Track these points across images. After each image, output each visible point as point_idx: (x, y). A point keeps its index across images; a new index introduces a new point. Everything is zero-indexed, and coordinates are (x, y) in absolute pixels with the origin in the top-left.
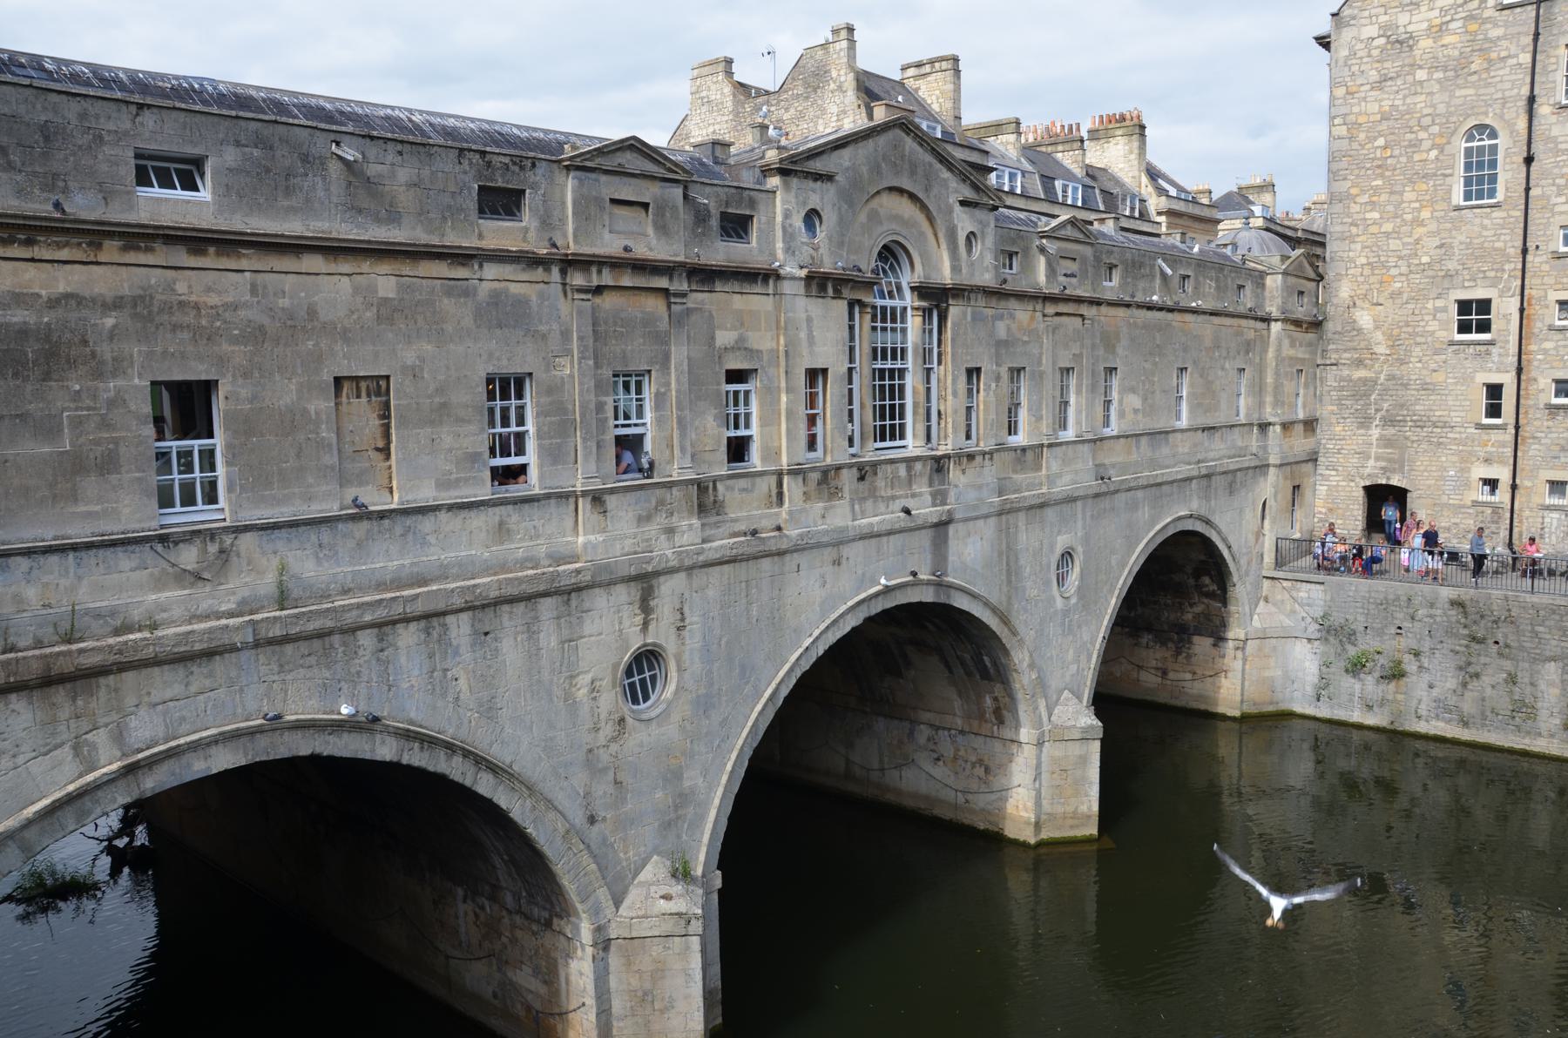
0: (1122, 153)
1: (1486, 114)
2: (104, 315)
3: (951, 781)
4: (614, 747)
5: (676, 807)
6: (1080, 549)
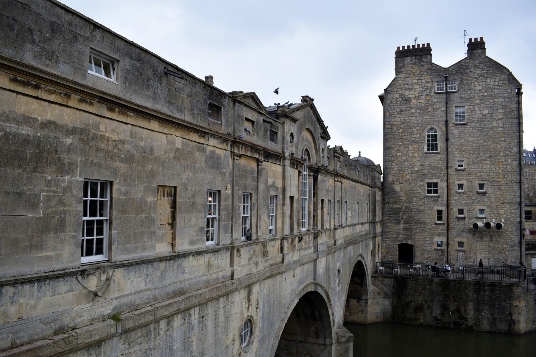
1: (434, 124)
2: (67, 136)
6: (341, 268)
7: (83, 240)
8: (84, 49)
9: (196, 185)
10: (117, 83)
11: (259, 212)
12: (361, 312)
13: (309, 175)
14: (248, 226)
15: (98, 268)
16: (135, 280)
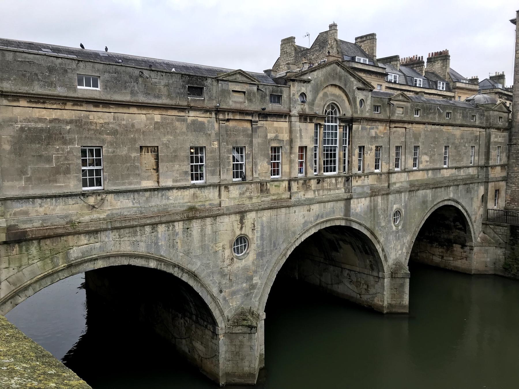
0: (440, 66)
3: (356, 290)
4: (229, 268)
5: (250, 289)
6: (403, 210)
9: (177, 144)
12: (465, 259)
13: (340, 126)
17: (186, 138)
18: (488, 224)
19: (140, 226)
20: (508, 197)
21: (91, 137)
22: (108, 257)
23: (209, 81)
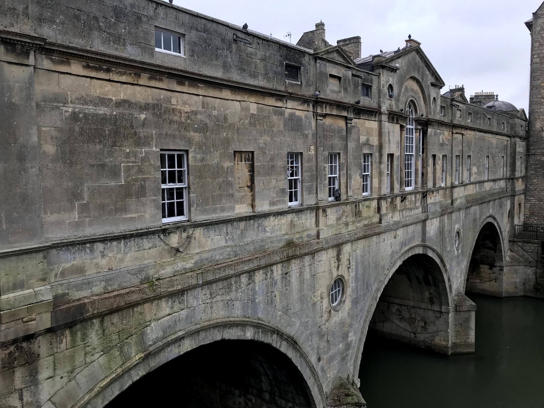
4: (327, 324)
6: (462, 230)
7: (164, 204)
8: (149, 28)
9: (274, 149)
10: (185, 57)
11: (349, 172)
12: (494, 281)
13: (416, 129)
14: (337, 187)
15: (178, 228)
16: (215, 238)
17: (284, 139)
18: (516, 242)
19: (236, 276)
20: (527, 211)
21: (173, 135)
22: (197, 332)
23: (307, 58)
